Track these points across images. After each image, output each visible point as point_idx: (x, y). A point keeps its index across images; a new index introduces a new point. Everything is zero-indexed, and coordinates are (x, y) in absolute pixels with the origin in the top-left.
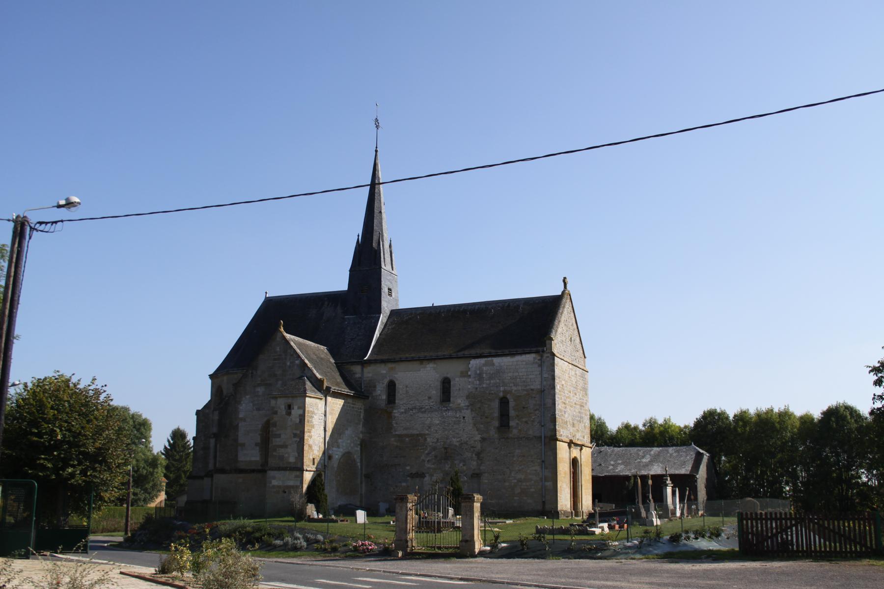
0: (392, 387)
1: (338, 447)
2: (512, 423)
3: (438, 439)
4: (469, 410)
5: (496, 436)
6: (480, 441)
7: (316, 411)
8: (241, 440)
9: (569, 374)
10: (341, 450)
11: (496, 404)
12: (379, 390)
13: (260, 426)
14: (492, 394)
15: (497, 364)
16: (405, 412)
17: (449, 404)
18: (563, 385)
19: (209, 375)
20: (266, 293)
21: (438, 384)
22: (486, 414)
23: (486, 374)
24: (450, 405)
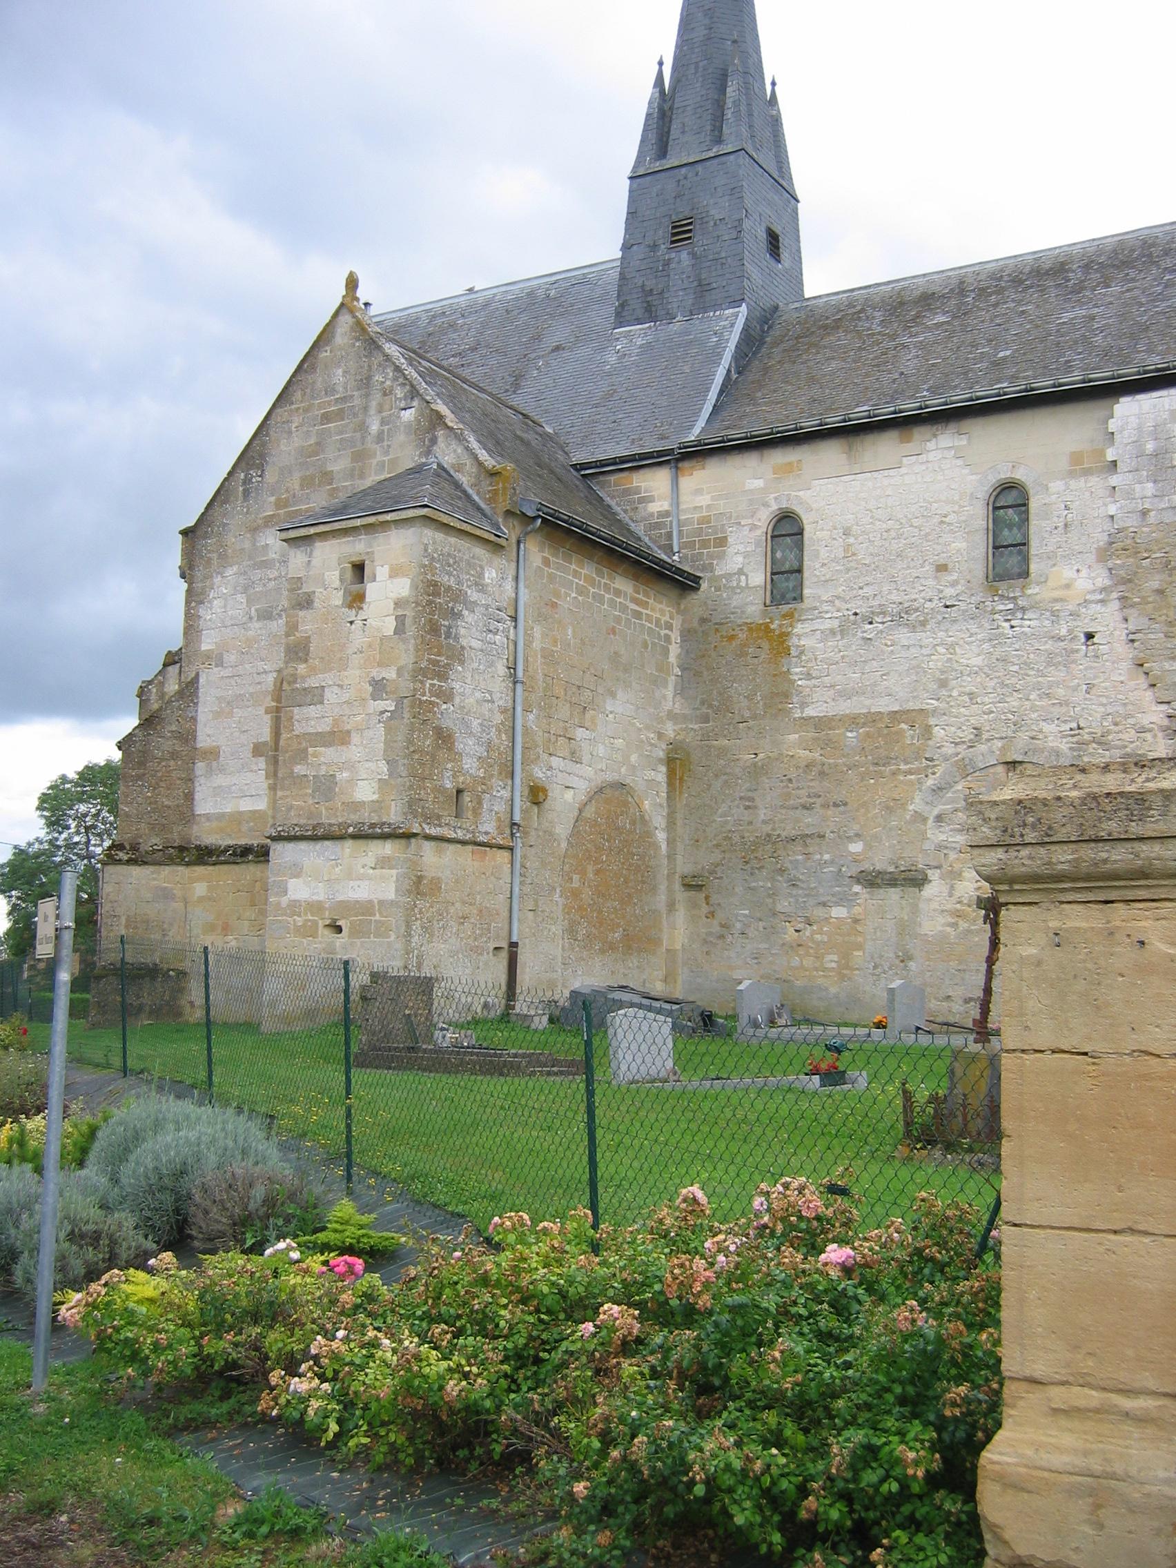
1: (575, 757)
4: (1115, 605)
6: (1164, 729)
7: (473, 595)
10: (588, 771)
16: (843, 631)
21: (978, 516)
24: (1029, 592)
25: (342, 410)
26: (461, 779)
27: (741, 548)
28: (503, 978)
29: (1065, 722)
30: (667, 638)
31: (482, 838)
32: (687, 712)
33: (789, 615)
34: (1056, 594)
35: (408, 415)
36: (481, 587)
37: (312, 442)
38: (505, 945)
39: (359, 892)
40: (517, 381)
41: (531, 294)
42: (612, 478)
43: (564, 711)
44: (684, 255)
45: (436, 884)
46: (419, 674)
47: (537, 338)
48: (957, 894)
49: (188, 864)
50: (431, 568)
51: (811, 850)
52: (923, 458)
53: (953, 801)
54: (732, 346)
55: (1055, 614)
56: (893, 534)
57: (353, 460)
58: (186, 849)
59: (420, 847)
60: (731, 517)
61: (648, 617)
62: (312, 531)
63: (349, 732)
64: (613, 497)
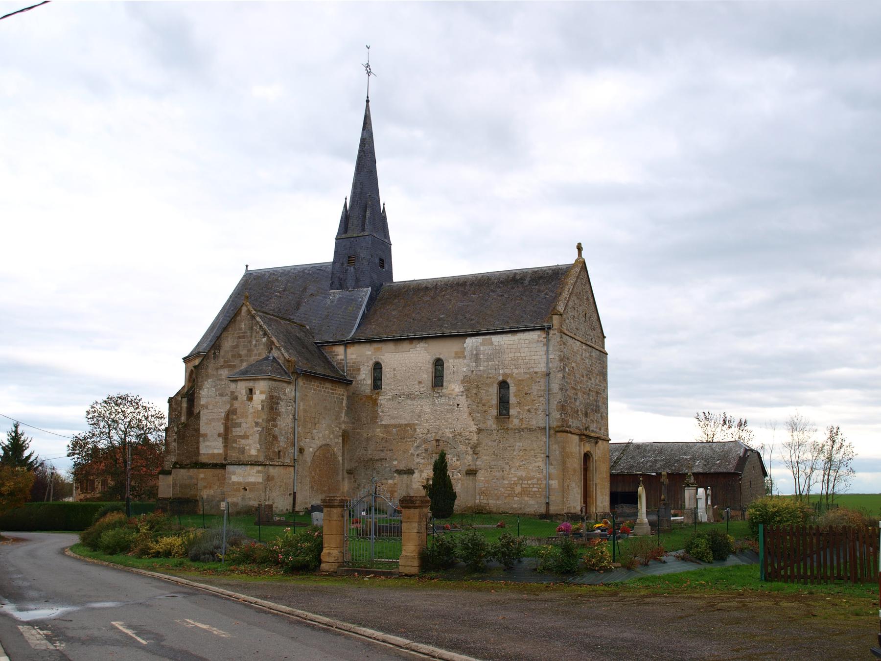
2: (512, 412)
3: (428, 431)
4: (465, 396)
5: (494, 426)
9: (582, 355)
11: (494, 390)
12: (363, 374)
13: (223, 415)
14: (490, 378)
15: (496, 343)
18: (573, 368)
19: (183, 359)
20: (247, 266)
21: (430, 367)
24: (443, 391)
25: (244, 336)
27: (364, 372)
28: (292, 502)
30: (343, 399)
31: (286, 464)
32: (348, 421)
33: (378, 393)
34: (450, 392)
35: (264, 340)
36: (285, 394)
37: (235, 344)
38: (292, 493)
39: (252, 479)
40: (298, 306)
42: (327, 347)
43: (310, 425)
44: (352, 268)
45: (273, 478)
46: (268, 421)
47: (305, 289)
48: (422, 477)
49: (198, 468)
51: (383, 463)
54: (365, 303)
57: (248, 352)
58: (197, 464)
59: (269, 468)
60: (361, 363)
61: (336, 394)
62: (238, 379)
64: (327, 353)
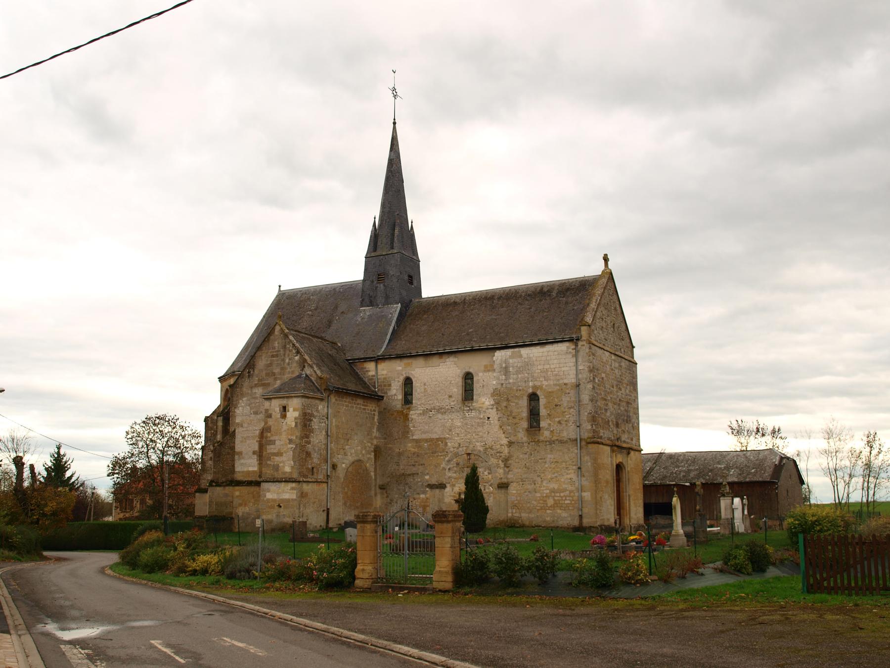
0: (408, 382)
4: (495, 409)
5: (525, 439)
7: (315, 414)
8: (238, 448)
9: (611, 366)
11: (524, 402)
14: (520, 390)
15: (525, 356)
17: (472, 403)
18: (603, 378)
19: (219, 378)
21: (459, 381)
22: (513, 414)
23: (513, 367)
24: (473, 405)
26: (313, 465)
29: (482, 442)
30: (374, 415)
31: (320, 481)
33: (409, 408)
36: (317, 411)
38: (326, 509)
39: (286, 496)
40: (330, 323)
41: (334, 289)
42: (358, 364)
44: (382, 285)
45: (307, 494)
46: (302, 438)
48: (454, 491)
49: (233, 486)
50: (304, 408)
51: (415, 478)
52: (445, 364)
53: (453, 464)
54: (395, 319)
55: (480, 412)
56: (437, 386)
57: (281, 370)
62: (271, 397)
63: (282, 453)
